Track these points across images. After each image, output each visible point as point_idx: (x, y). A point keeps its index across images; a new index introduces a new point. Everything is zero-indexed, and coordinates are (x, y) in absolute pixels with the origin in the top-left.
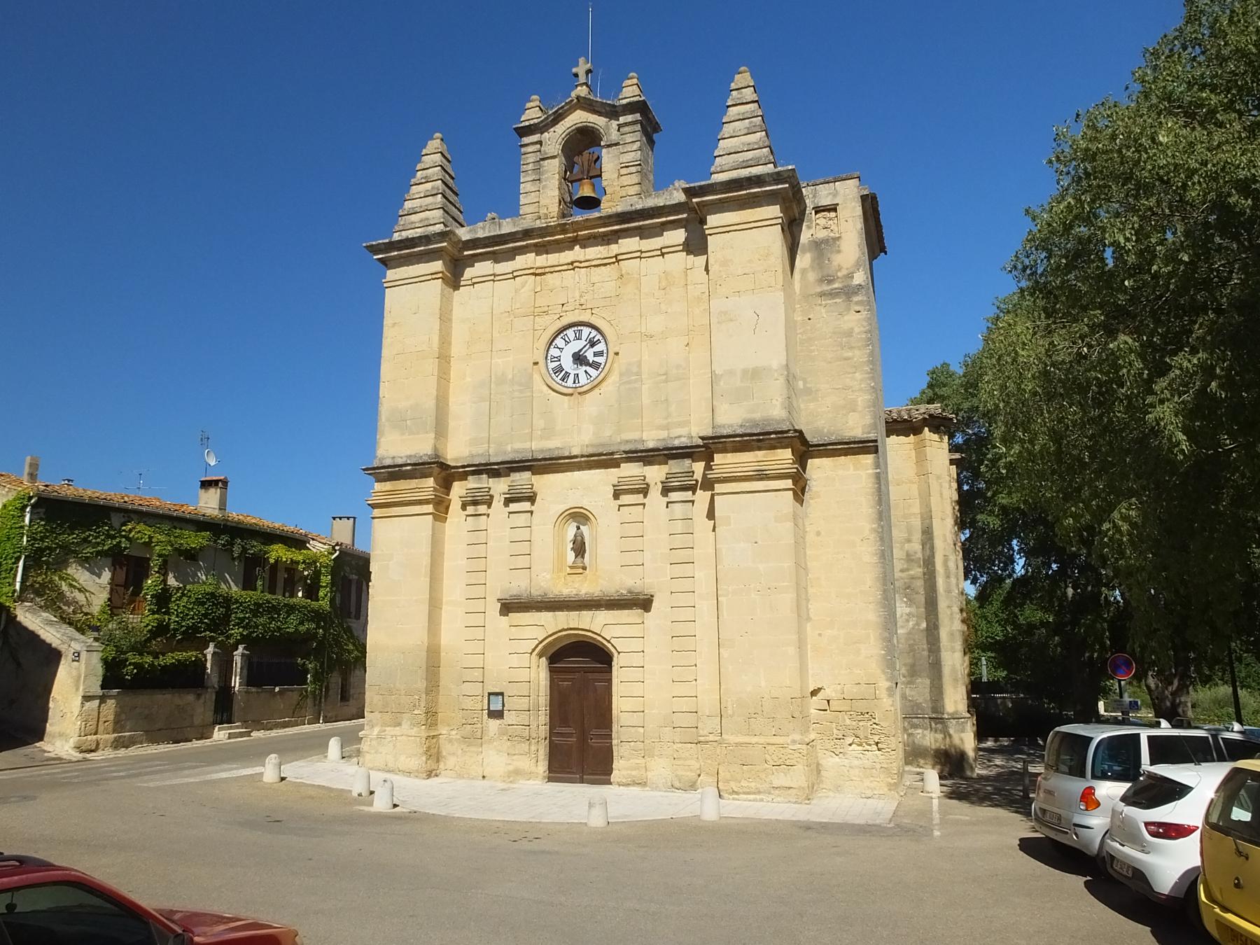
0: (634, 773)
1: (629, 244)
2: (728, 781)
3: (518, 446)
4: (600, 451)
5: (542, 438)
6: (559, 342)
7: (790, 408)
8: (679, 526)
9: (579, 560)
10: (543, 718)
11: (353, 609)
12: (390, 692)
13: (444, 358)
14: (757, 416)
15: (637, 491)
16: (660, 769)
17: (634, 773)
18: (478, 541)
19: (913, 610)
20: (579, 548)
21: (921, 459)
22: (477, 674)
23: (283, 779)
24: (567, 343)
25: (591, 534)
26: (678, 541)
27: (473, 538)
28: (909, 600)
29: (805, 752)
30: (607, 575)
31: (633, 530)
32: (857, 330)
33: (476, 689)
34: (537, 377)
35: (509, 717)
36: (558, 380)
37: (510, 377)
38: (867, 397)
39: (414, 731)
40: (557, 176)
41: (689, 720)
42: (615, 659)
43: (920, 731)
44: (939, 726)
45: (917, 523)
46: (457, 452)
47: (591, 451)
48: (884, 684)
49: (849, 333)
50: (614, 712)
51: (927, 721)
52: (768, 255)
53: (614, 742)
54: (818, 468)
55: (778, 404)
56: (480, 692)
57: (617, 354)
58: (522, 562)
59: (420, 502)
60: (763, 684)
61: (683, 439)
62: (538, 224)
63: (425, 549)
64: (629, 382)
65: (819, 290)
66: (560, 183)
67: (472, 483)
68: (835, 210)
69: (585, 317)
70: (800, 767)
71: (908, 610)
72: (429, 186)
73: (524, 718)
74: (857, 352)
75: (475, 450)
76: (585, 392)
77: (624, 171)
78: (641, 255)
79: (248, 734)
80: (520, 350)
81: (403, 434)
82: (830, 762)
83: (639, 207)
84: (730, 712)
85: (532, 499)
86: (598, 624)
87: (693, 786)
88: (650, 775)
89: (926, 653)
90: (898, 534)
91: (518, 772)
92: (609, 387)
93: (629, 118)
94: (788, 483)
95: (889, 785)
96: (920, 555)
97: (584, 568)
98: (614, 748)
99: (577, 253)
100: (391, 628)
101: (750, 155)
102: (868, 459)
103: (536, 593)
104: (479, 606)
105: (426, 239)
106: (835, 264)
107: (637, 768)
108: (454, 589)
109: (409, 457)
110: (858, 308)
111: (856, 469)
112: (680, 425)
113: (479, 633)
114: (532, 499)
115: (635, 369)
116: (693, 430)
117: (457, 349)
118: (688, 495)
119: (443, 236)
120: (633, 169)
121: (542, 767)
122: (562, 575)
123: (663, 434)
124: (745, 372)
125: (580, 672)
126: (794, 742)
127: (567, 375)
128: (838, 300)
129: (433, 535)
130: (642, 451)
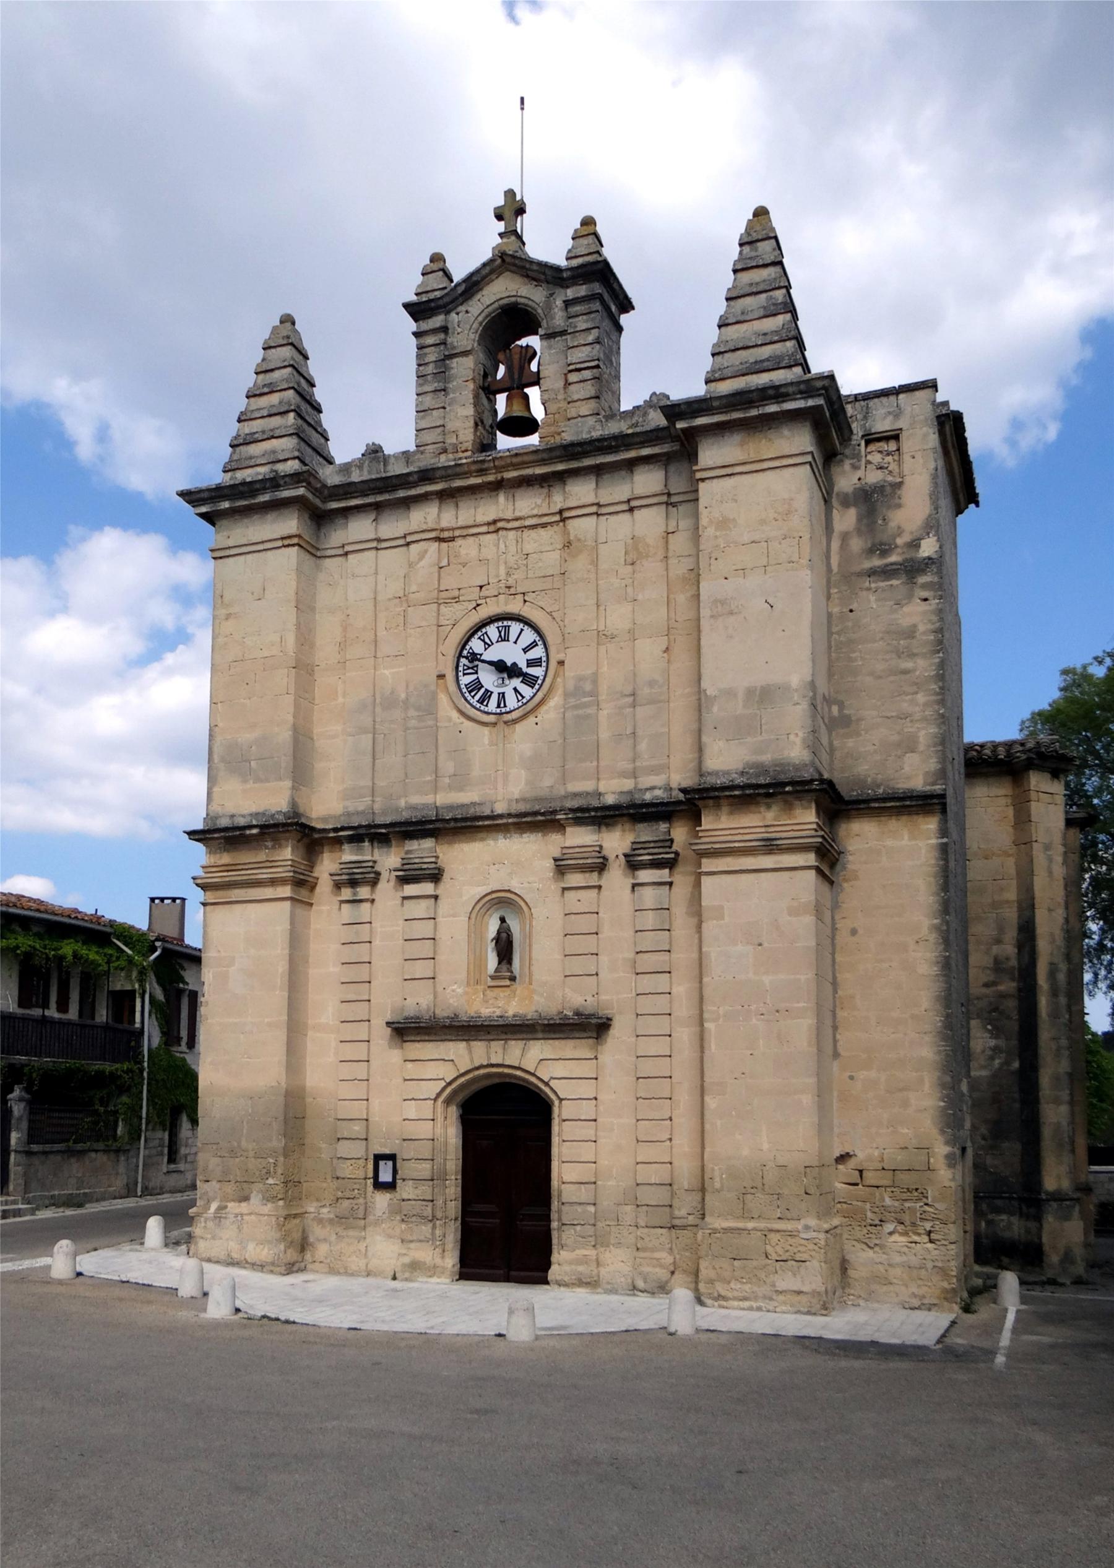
0: (581, 1268)
1: (582, 491)
3: (416, 799)
4: (537, 808)
5: (450, 788)
7: (814, 746)
8: (649, 920)
9: (504, 967)
10: (453, 1189)
11: (184, 1033)
12: (233, 1153)
13: (304, 669)
14: (766, 758)
16: (617, 1263)
17: (581, 1268)
18: (358, 938)
19: (1001, 1043)
20: (505, 947)
21: (1022, 819)
22: (357, 1128)
23: (79, 1274)
24: (487, 646)
25: (523, 930)
26: (648, 941)
27: (349, 934)
28: (995, 1027)
29: (823, 1242)
31: (585, 924)
32: (921, 628)
33: (356, 1150)
34: (443, 698)
35: (406, 1190)
37: (403, 696)
38: (933, 730)
39: (268, 1208)
41: (658, 1196)
42: (556, 1110)
43: (1004, 1217)
44: (1032, 1211)
45: (1011, 915)
46: (326, 806)
47: (522, 807)
48: (941, 1149)
49: (910, 633)
50: (555, 1183)
51: (1015, 1203)
52: (788, 513)
53: (554, 1225)
54: (862, 837)
55: (798, 741)
57: (561, 663)
58: (421, 969)
59: (273, 882)
60: (765, 1146)
61: (658, 793)
62: (444, 460)
63: (279, 951)
64: (576, 707)
65: (867, 564)
66: (476, 397)
67: (349, 854)
68: (896, 438)
69: (514, 606)
71: (993, 1043)
72: (275, 399)
73: (425, 1191)
74: (921, 663)
76: (515, 721)
77: (573, 377)
78: (598, 510)
79: (33, 1212)
80: (416, 658)
81: (245, 781)
82: (862, 1258)
83: (596, 434)
84: (717, 1185)
85: (436, 876)
86: (539, 1061)
87: (663, 1288)
88: (603, 1271)
89: (1017, 1105)
90: (982, 930)
91: (415, 1266)
92: (550, 713)
93: (582, 291)
94: (811, 859)
96: (1014, 963)
97: (513, 979)
99: (499, 506)
100: (233, 1057)
101: (766, 352)
102: (930, 825)
103: (442, 1013)
105: (274, 482)
106: (892, 524)
107: (584, 1260)
108: (325, 1007)
109: (256, 815)
111: (913, 837)
112: (654, 770)
113: (360, 1071)
114: (436, 876)
115: (588, 687)
117: (325, 652)
118: (663, 874)
119: (296, 478)
120: (587, 374)
121: (451, 1260)
122: (480, 988)
123: (628, 784)
124: (750, 692)
127: (488, 694)
128: (895, 582)
130: (596, 809)
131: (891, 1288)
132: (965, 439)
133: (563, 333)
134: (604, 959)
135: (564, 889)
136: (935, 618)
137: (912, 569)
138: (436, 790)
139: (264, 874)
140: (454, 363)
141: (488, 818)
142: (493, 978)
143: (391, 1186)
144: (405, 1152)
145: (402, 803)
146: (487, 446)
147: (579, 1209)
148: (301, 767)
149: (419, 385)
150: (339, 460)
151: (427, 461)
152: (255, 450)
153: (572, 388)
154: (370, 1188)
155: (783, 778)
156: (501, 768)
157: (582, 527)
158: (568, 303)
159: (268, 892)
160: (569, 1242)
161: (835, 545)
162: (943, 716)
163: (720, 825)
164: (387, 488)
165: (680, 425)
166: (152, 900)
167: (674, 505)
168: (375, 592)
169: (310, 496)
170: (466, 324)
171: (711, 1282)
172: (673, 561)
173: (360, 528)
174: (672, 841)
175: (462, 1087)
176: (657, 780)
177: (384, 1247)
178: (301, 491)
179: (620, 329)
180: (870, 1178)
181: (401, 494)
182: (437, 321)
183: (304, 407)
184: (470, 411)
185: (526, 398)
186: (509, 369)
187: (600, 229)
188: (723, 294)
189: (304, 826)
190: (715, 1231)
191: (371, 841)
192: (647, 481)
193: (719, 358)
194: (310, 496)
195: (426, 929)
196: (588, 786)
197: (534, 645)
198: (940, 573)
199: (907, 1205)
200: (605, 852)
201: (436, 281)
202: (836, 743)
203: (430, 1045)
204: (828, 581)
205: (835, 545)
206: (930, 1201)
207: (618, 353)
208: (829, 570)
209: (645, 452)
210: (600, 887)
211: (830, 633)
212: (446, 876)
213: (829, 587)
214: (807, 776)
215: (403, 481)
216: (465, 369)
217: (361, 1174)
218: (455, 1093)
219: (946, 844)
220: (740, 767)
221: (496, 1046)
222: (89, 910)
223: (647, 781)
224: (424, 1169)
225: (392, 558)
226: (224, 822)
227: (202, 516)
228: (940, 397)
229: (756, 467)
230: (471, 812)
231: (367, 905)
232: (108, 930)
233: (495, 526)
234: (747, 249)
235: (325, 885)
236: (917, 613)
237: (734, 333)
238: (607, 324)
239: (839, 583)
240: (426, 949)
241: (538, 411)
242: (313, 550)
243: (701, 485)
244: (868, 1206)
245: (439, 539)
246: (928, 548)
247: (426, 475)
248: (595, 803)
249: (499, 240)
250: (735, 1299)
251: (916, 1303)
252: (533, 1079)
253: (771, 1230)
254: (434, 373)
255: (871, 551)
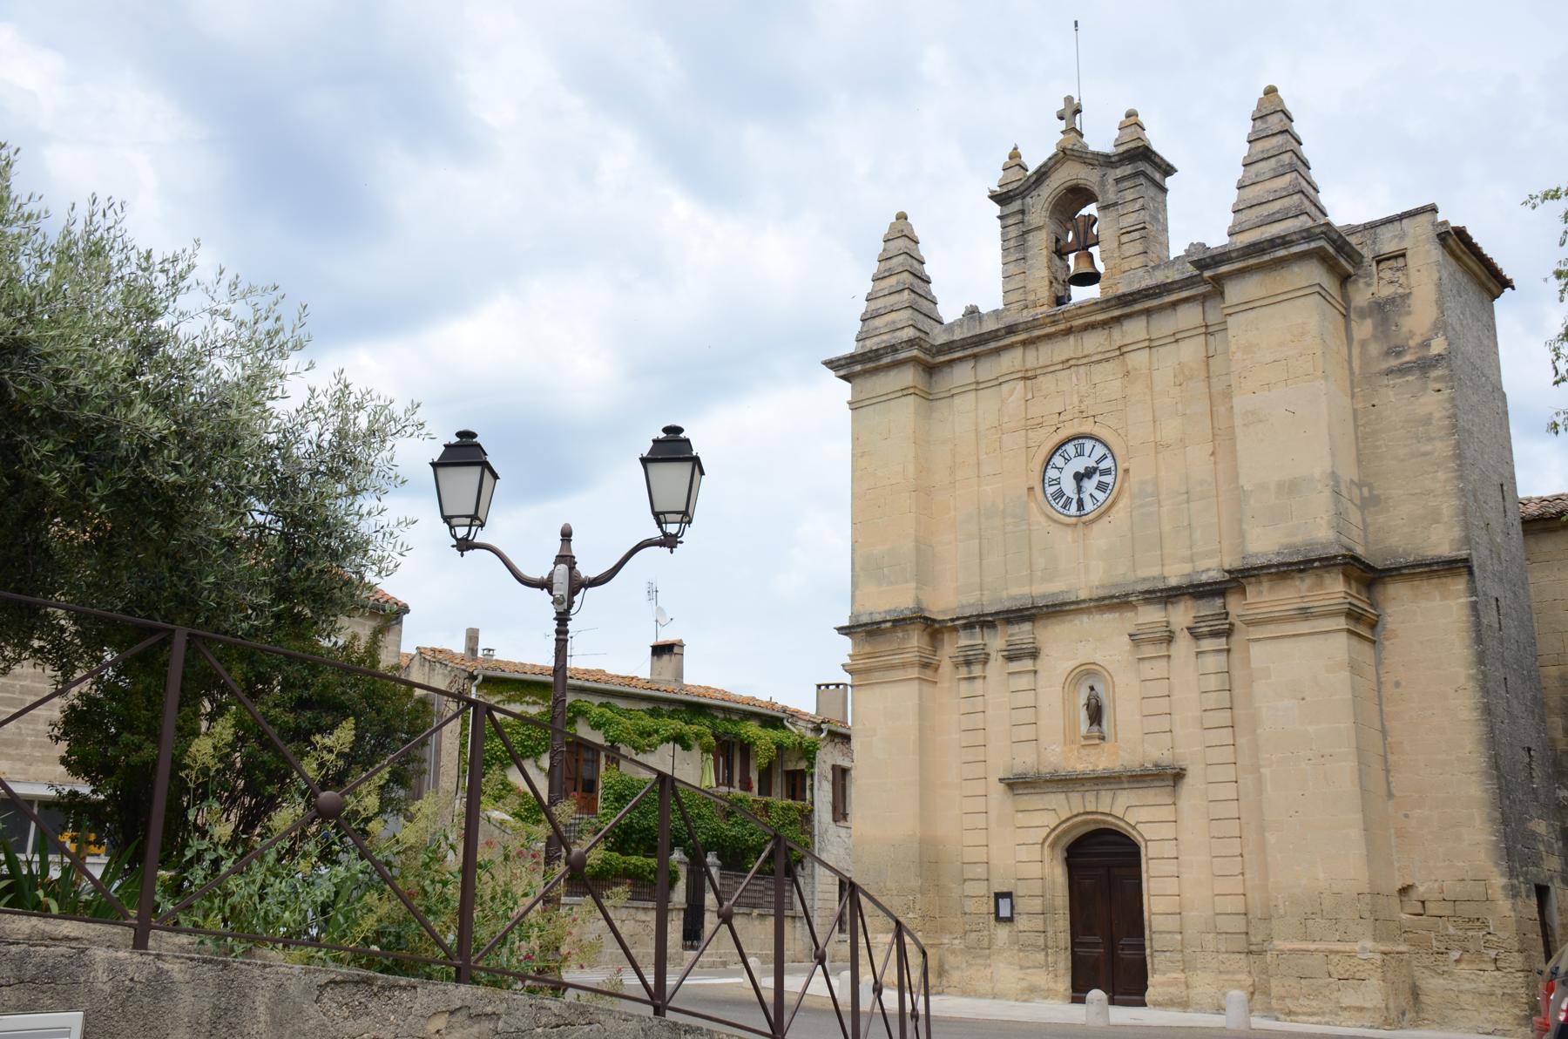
0: (1172, 990)
1: (1135, 330)
2: (1282, 998)
3: (1015, 591)
6: (1058, 460)
9: (1095, 728)
10: (1063, 923)
14: (1298, 539)
15: (1160, 641)
16: (1203, 985)
17: (1172, 990)
20: (1096, 713)
22: (980, 871)
24: (1067, 460)
27: (967, 706)
30: (1129, 743)
32: (1437, 415)
33: (979, 889)
34: (1033, 505)
35: (1022, 923)
36: (1058, 507)
40: (1045, 252)
46: (945, 602)
47: (1102, 593)
48: (1499, 881)
49: (1427, 420)
53: (1148, 951)
56: (983, 891)
57: (1126, 471)
58: (1026, 733)
59: (904, 665)
60: (1321, 876)
62: (1026, 316)
64: (1141, 506)
65: (1384, 366)
66: (1050, 260)
67: (964, 640)
68: (1403, 255)
69: (1087, 428)
70: (1374, 981)
72: (893, 280)
73: (1038, 923)
74: (1439, 445)
75: (964, 600)
77: (1125, 239)
82: (1432, 984)
83: (1143, 285)
84: (1282, 911)
85: (1034, 654)
86: (1133, 812)
88: (1192, 993)
93: (1128, 170)
94: (1342, 623)
95: (1517, 1017)
97: (1103, 739)
98: (1149, 960)
101: (1277, 206)
102: (1459, 585)
103: (1046, 770)
104: (979, 787)
105: (894, 349)
106: (1404, 329)
107: (1174, 983)
109: (888, 612)
110: (1438, 386)
114: (1034, 654)
116: (1210, 568)
119: (911, 343)
120: (1136, 235)
123: (1187, 568)
125: (1103, 872)
126: (1364, 949)
127: (1069, 500)
128: (1410, 378)
129: (921, 706)
130: (1161, 591)
131: (1463, 1013)
132: (1475, 245)
133: (1115, 204)
134: (1176, 717)
135: (1198, 653)
136: (1448, 406)
137: (1425, 365)
138: (1031, 582)
139: (897, 659)
140: (1030, 237)
141: (1073, 603)
142: (1086, 738)
143: (1010, 920)
144: (1020, 890)
145: (1004, 594)
146: (1060, 300)
147: (1168, 936)
148: (924, 568)
149: (1004, 257)
150: (947, 321)
151: (1009, 319)
152: (878, 322)
153: (1124, 247)
154: (993, 922)
155: (1313, 555)
156: (1082, 564)
157: (1138, 359)
158: (1117, 181)
159: (900, 675)
160: (1161, 967)
161: (1356, 351)
162: (1462, 490)
163: (1263, 599)
164: (982, 342)
165: (1207, 274)
166: (819, 686)
167: (1212, 334)
168: (977, 424)
169: (921, 355)
170: (1039, 207)
171: (1282, 998)
172: (1214, 380)
173: (962, 374)
174: (1227, 614)
175: (1065, 832)
176: (1213, 563)
177: (1006, 972)
178: (915, 352)
179: (1164, 190)
180: (1432, 908)
181: (993, 345)
182: (1016, 205)
183: (917, 282)
184: (1045, 273)
185: (1091, 256)
186: (1076, 235)
187: (1141, 118)
188: (1241, 162)
189: (926, 618)
190: (1282, 952)
191: (982, 628)
192: (1189, 316)
193: (1239, 215)
194: (921, 355)
195: (1028, 698)
196: (1155, 571)
197: (1104, 457)
198: (1449, 366)
199: (1470, 933)
200: (1172, 628)
201: (1016, 174)
202: (1369, 520)
203: (1035, 797)
204: (1352, 381)
205: (1356, 351)
206: (1491, 930)
207: (1165, 210)
208: (1352, 372)
209: (1184, 294)
210: (1169, 656)
211: (1356, 426)
212: (1042, 655)
213: (1352, 388)
214: (1333, 552)
215: (993, 335)
216: (1041, 243)
217: (984, 909)
218: (1058, 838)
219: (1475, 603)
220: (1276, 548)
221: (1090, 796)
222: (765, 698)
223: (1202, 564)
224: (1037, 904)
225: (989, 399)
226: (865, 619)
227: (842, 377)
228: (1440, 218)
229: (1274, 300)
230: (1060, 599)
231: (981, 681)
232: (780, 715)
233: (1068, 364)
234: (1259, 123)
235: (946, 666)
236: (1432, 402)
237: (1252, 193)
238: (1152, 191)
239: (1362, 382)
240: (1028, 715)
241: (1100, 267)
242: (928, 397)
243: (1229, 319)
244: (1433, 935)
245: (1026, 378)
246: (1438, 346)
247: (1011, 330)
248: (1161, 586)
249: (1062, 136)
250: (1304, 1014)
251: (1490, 1028)
252: (1122, 824)
253: (1331, 952)
254: (1016, 246)
255: (1387, 354)
